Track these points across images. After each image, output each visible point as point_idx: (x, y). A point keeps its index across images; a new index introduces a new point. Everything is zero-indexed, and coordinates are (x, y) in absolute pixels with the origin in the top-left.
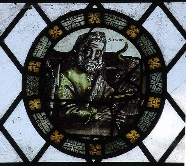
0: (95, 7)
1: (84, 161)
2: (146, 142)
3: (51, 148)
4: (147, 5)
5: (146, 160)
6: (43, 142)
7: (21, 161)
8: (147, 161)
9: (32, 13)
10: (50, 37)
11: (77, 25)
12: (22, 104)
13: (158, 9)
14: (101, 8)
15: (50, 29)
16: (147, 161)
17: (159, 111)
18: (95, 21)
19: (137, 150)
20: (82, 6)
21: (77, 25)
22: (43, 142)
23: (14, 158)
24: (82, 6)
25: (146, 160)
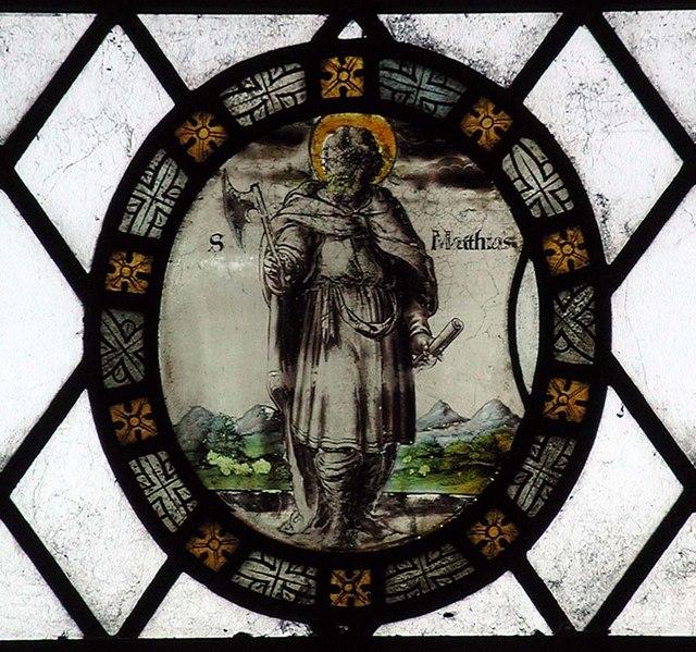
0: (352, 32)
1: (301, 630)
2: (541, 556)
3: (185, 584)
4: (542, 22)
5: (537, 623)
6: (155, 558)
7: (75, 633)
8: (145, 19)
9: (579, 601)
10: (512, 512)
11: (283, 106)
12: (82, 406)
13: (582, 41)
14: (375, 31)
15: (516, 542)
16: (145, 19)
17: (582, 434)
18: (343, 90)
19: (196, 69)
20: (300, 28)
21: (283, 106)
22: (155, 558)
23: (53, 622)
24: (300, 28)
25: (537, 623)
